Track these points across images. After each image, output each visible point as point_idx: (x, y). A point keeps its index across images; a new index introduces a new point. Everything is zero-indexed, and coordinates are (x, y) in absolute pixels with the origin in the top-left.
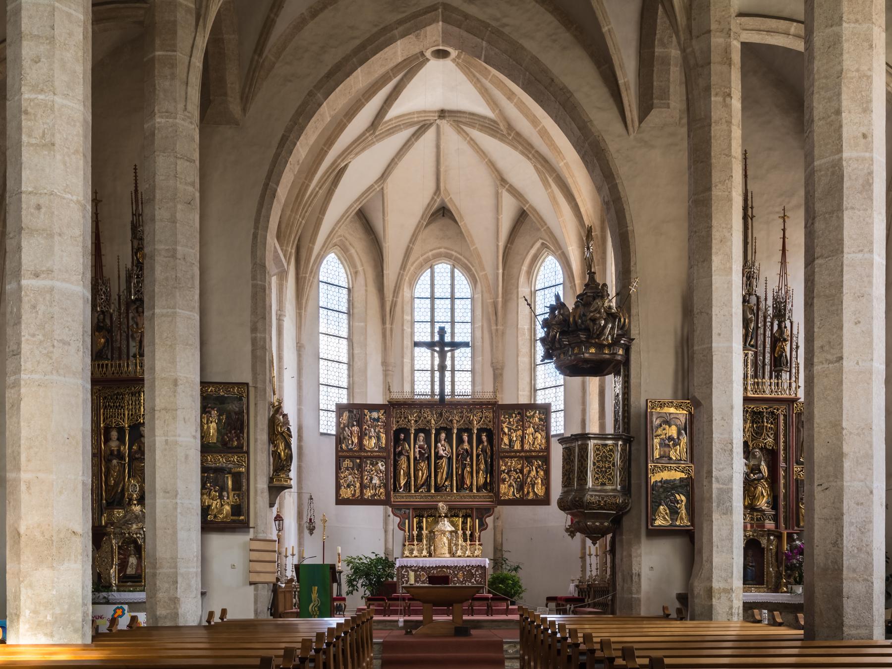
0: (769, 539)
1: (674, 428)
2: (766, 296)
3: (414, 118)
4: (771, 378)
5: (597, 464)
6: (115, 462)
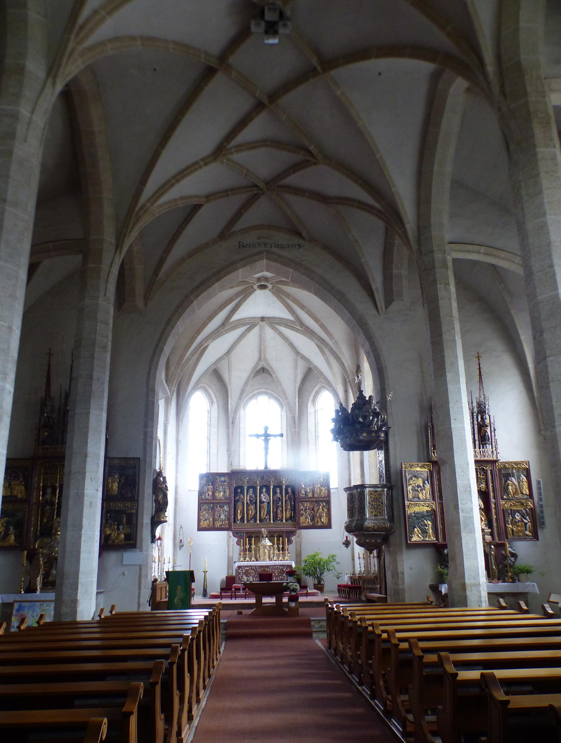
0: (491, 548)
1: (420, 480)
2: (472, 401)
3: (247, 321)
4: (480, 448)
5: (371, 503)
6: (48, 507)
